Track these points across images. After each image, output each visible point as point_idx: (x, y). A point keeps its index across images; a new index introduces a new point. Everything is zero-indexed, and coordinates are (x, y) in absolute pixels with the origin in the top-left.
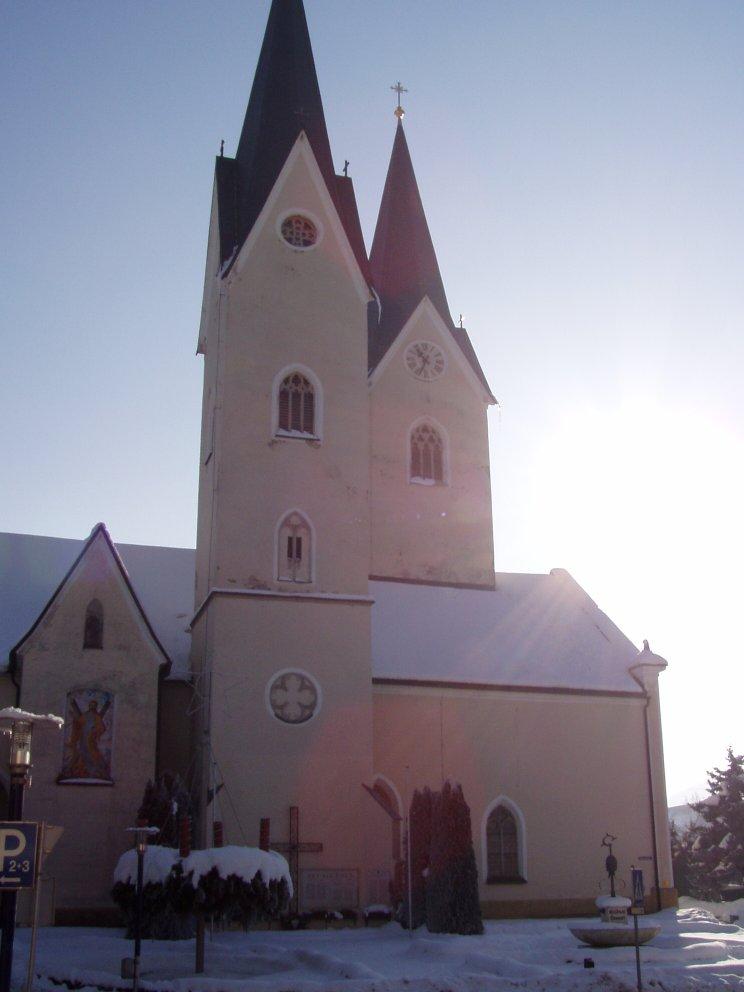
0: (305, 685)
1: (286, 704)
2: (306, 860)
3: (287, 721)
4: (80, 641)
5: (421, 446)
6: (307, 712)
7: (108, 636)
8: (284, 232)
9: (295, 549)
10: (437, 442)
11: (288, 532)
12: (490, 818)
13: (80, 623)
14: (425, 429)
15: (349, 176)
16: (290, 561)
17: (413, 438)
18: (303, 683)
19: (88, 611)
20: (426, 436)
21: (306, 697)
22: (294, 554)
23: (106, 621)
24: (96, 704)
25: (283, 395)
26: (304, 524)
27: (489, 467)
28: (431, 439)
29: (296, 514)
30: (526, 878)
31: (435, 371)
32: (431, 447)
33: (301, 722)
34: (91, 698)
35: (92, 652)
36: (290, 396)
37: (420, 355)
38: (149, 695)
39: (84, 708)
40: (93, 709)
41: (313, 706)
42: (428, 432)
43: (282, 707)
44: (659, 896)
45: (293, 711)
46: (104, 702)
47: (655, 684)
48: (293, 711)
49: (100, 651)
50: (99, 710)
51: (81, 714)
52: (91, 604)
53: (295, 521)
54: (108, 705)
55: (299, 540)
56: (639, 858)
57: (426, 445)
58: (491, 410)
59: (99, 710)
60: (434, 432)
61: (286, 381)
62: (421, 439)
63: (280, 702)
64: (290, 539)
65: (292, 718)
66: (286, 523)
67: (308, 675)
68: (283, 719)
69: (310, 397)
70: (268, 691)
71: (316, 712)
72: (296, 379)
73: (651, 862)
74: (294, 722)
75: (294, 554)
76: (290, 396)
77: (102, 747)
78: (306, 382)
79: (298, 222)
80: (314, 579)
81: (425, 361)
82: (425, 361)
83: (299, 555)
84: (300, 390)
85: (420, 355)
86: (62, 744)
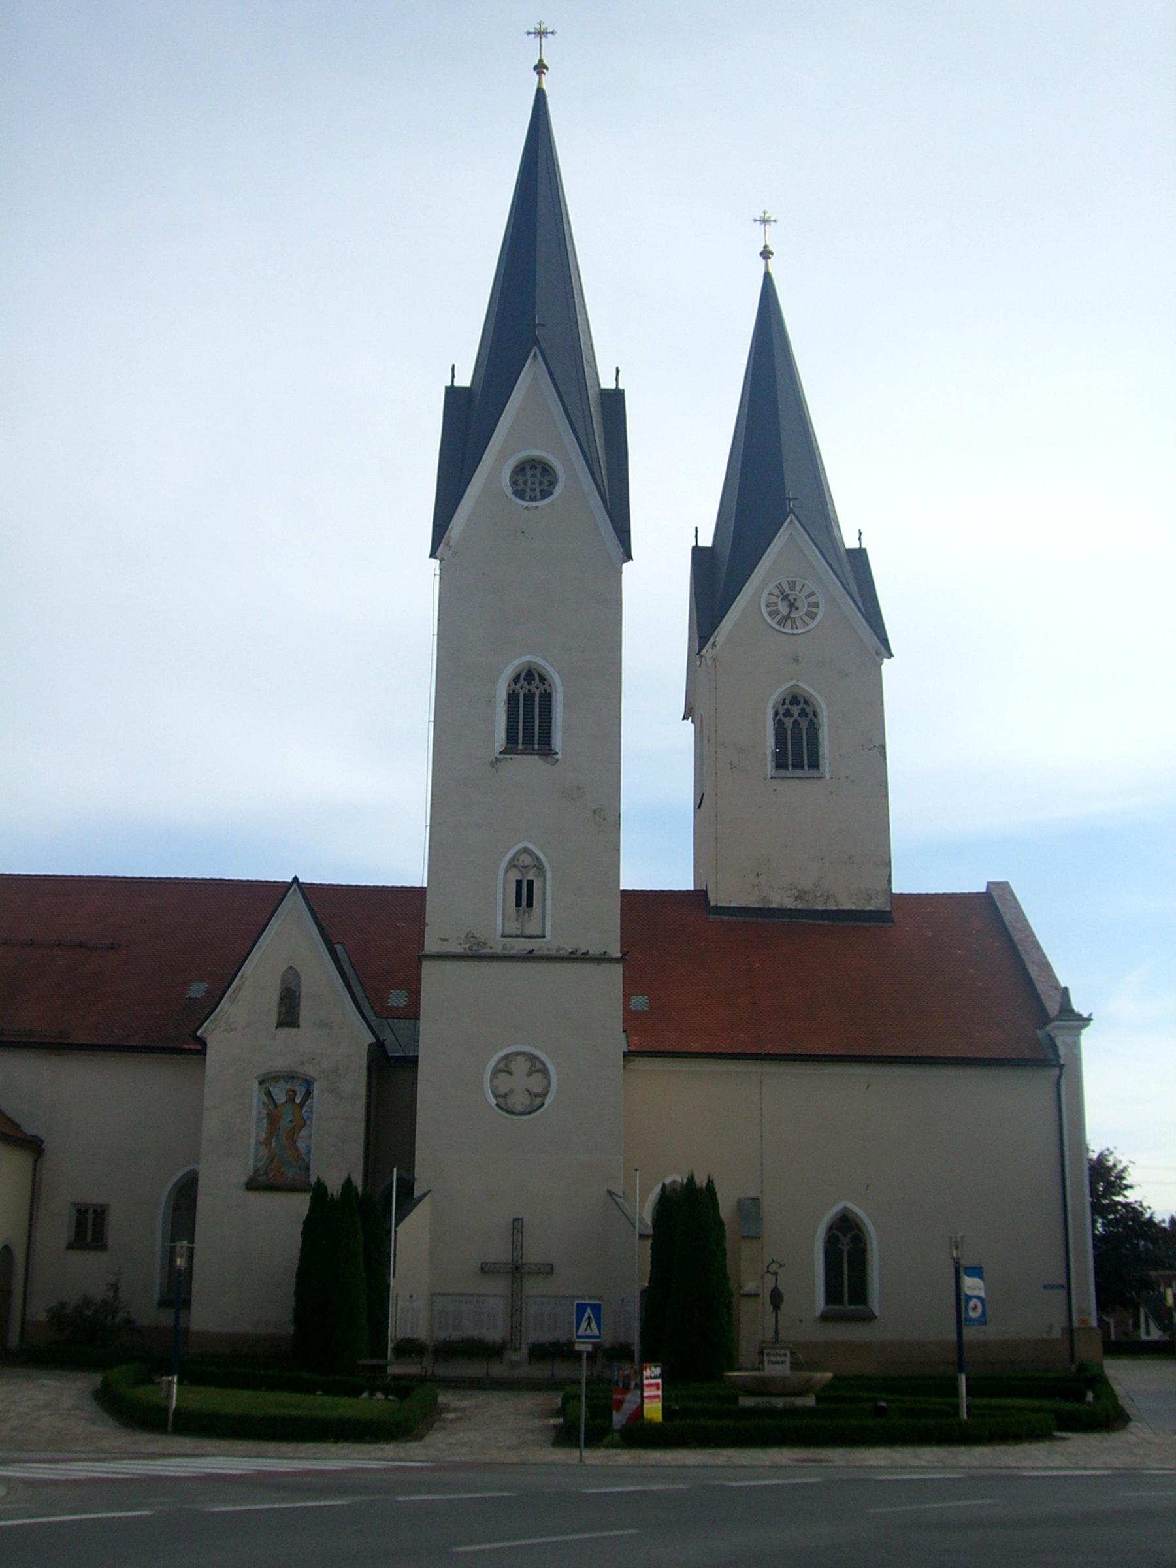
0: (537, 1067)
1: (512, 1091)
2: (533, 1287)
3: (512, 1113)
4: (273, 1019)
5: (789, 723)
6: (538, 1101)
7: (306, 1012)
8: (514, 483)
9: (525, 895)
10: (811, 716)
11: (515, 875)
12: (830, 1229)
13: (272, 996)
14: (795, 700)
15: (621, 387)
16: (518, 911)
17: (776, 714)
18: (500, 1071)
19: (283, 981)
20: (795, 710)
21: (536, 1082)
22: (524, 903)
23: (303, 992)
24: (295, 1092)
25: (512, 698)
26: (539, 867)
27: (883, 747)
28: (803, 713)
29: (526, 850)
30: (877, 1314)
31: (806, 619)
32: (804, 725)
33: (529, 1113)
34: (288, 1086)
35: (285, 1031)
36: (537, 699)
37: (785, 597)
38: (356, 1083)
39: (280, 1098)
40: (291, 1099)
41: (544, 1095)
42: (798, 703)
43: (505, 1096)
44: (1072, 1340)
45: (519, 1100)
46: (304, 1090)
47: (1076, 1045)
48: (519, 1100)
49: (295, 1030)
50: (298, 1101)
51: (276, 1106)
52: (286, 971)
53: (526, 860)
54: (309, 1093)
55: (530, 884)
56: (1045, 1287)
57: (796, 722)
58: (887, 665)
59: (298, 1101)
60: (806, 702)
61: (516, 679)
62: (788, 713)
63: (502, 1091)
64: (519, 883)
65: (519, 1108)
66: (512, 864)
67: (536, 1052)
68: (507, 1112)
69: (547, 698)
70: (487, 1077)
71: (547, 1102)
72: (530, 675)
73: (1062, 1293)
74: (521, 1114)
75: (524, 903)
76: (537, 699)
77: (301, 1145)
78: (543, 679)
79: (533, 467)
80: (548, 933)
81: (792, 606)
82: (792, 606)
83: (530, 904)
84: (533, 689)
85: (785, 597)
86: (253, 1141)
